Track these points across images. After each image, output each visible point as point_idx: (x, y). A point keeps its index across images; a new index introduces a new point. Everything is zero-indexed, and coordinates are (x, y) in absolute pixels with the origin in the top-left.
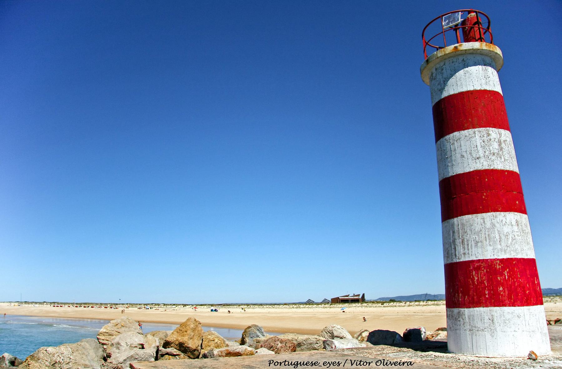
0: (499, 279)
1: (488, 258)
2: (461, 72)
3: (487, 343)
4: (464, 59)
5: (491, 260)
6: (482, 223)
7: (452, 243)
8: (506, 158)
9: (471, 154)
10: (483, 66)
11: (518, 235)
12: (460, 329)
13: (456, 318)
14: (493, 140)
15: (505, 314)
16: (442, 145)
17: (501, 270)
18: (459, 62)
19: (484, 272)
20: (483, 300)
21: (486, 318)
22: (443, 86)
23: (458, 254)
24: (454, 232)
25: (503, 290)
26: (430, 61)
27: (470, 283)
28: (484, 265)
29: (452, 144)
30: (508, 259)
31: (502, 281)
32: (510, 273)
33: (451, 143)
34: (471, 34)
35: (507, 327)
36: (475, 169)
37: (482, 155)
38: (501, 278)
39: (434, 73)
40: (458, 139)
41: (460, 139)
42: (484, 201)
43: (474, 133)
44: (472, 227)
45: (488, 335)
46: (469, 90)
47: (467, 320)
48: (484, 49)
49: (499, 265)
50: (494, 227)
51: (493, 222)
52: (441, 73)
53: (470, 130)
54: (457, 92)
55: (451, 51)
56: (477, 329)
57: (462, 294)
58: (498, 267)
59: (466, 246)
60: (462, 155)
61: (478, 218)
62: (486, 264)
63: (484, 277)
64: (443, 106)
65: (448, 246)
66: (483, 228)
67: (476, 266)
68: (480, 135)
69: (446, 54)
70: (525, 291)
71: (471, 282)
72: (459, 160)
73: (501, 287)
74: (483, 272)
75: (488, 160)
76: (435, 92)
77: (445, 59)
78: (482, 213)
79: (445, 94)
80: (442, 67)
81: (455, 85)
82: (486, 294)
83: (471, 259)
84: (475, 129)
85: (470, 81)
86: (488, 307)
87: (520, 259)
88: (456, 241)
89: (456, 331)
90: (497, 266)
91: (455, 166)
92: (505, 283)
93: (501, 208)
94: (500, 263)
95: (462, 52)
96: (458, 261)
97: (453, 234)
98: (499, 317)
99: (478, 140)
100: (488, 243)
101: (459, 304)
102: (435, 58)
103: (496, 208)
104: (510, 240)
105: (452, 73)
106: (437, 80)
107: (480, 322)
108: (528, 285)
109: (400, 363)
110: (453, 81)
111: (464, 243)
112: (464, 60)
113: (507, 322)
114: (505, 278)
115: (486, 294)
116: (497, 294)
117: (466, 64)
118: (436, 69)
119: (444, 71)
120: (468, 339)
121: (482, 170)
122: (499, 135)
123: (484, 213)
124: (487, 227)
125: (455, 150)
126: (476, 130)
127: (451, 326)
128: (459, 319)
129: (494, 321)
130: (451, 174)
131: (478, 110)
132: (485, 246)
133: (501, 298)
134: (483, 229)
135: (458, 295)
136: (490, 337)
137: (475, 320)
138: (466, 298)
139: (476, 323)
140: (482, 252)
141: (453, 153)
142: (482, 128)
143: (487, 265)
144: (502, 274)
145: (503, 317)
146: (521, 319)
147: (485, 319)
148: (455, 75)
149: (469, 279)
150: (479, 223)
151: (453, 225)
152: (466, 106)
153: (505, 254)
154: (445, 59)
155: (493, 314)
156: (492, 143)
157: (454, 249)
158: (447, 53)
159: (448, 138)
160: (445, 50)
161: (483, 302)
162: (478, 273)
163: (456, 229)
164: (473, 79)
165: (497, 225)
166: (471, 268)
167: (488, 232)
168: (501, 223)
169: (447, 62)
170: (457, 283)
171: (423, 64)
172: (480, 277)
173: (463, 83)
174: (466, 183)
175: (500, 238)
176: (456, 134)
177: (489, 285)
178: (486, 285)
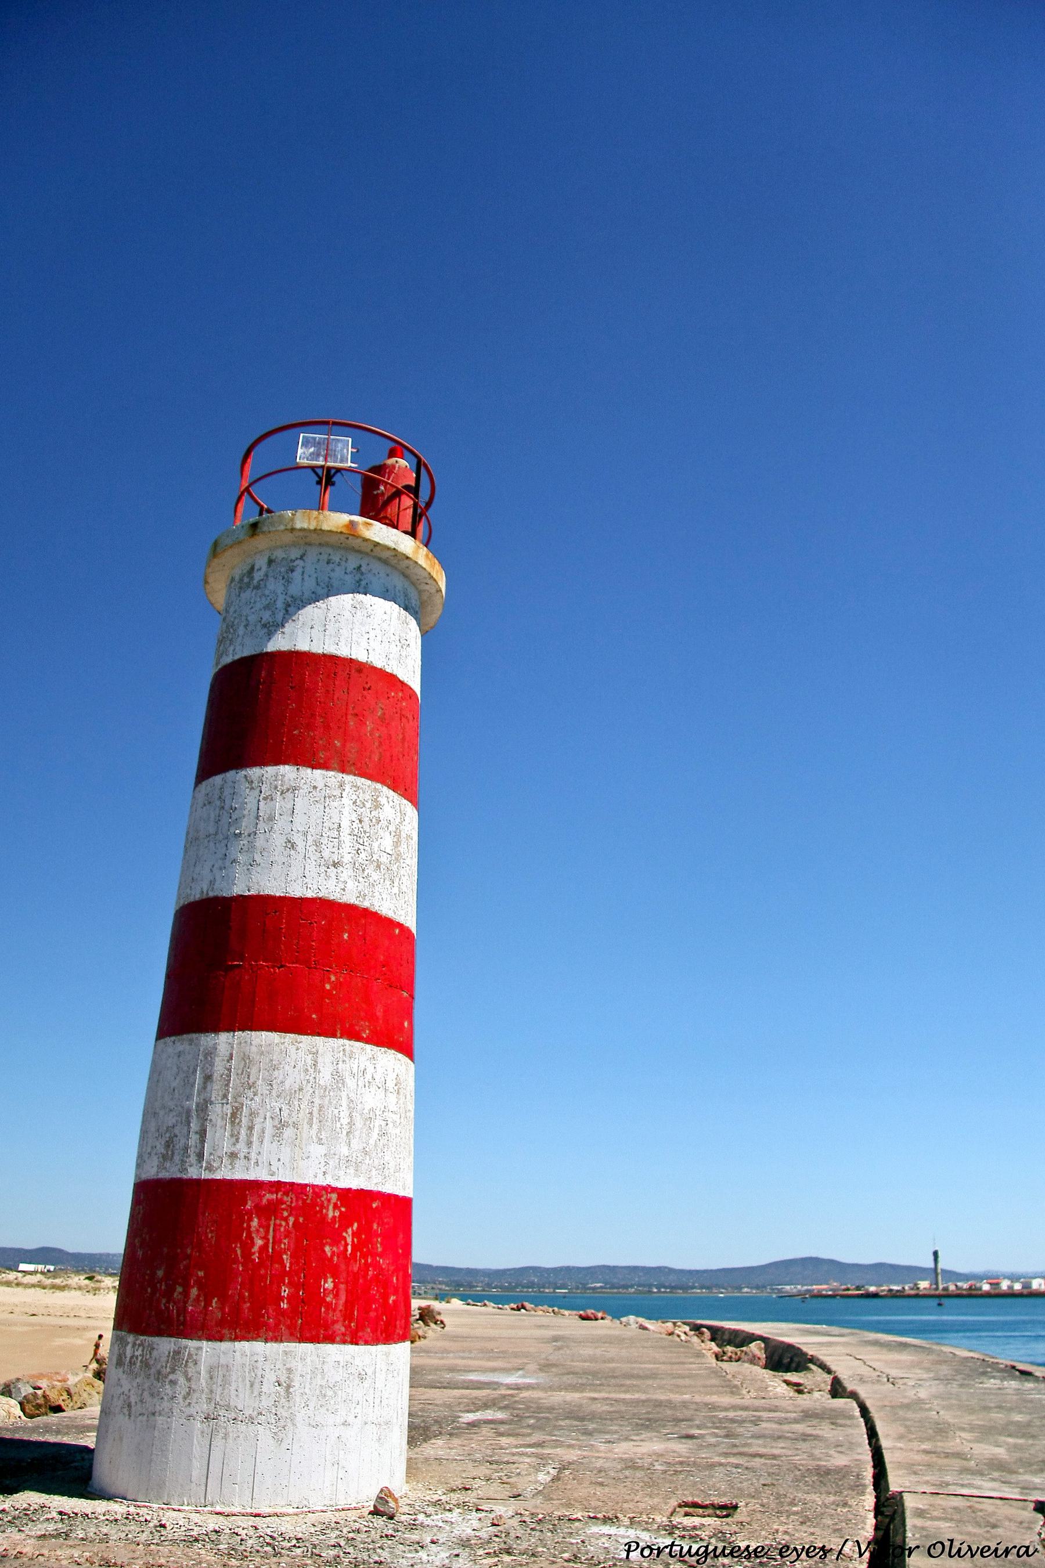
0: (329, 1254)
1: (306, 1182)
2: (346, 600)
3: (258, 1464)
4: (360, 566)
5: (313, 1186)
6: (309, 1068)
7: (194, 1114)
8: (404, 889)
9: (317, 844)
10: (402, 609)
11: (394, 1122)
12: (170, 1414)
13: (159, 1372)
14: (384, 823)
15: (325, 1367)
16: (227, 791)
17: (337, 1226)
18: (346, 569)
19: (288, 1224)
20: (269, 1318)
21: (271, 1377)
22: (279, 616)
23: (211, 1154)
24: (208, 1078)
25: (333, 1290)
26: (265, 529)
27: (236, 1255)
28: (291, 1202)
29: (265, 799)
30: (361, 1192)
31: (335, 1259)
32: (359, 1238)
33: (263, 795)
34: (389, 510)
35: (328, 1410)
36: (320, 895)
37: (347, 859)
38: (335, 1249)
39: (260, 569)
40: (288, 790)
41: (295, 789)
42: (327, 1001)
43: (341, 785)
44: (276, 1073)
45: (264, 1434)
46: (353, 657)
47: (203, 1381)
48: (420, 562)
49: (336, 1207)
50: (340, 1085)
51: (340, 1070)
52: (283, 578)
53: (331, 773)
54: (320, 651)
55: (338, 528)
56: (233, 1415)
57: (199, 1289)
58: (331, 1214)
59: (243, 1132)
60: (290, 842)
61: (298, 1049)
62: (297, 1201)
63: (286, 1241)
64: (263, 674)
65: (174, 1121)
66: (308, 1081)
67: (264, 1201)
68: (354, 797)
69: (321, 530)
70: (385, 1297)
71: (239, 1252)
72: (278, 853)
73: (330, 1280)
74: (284, 1223)
75: (361, 879)
76: (246, 626)
77: (310, 544)
78: (313, 1033)
79: (279, 643)
80: (293, 561)
81: (318, 627)
82: (282, 1298)
83: (251, 1176)
84: (344, 775)
85: (364, 634)
86: (282, 1341)
87: (390, 1195)
88: (210, 1107)
89: (152, 1418)
90: (328, 1209)
91: (259, 869)
92: (343, 1267)
93: (367, 1032)
94: (338, 1200)
95: (365, 544)
96: (205, 1175)
97: (205, 1083)
98: (309, 1377)
99: (346, 811)
100: (314, 1132)
101: (184, 1323)
102: (282, 527)
103: (357, 1028)
104: (375, 1135)
105: (320, 591)
106: (267, 592)
107: (248, 1392)
108: (395, 1279)
109: (996, 1550)
110: (315, 615)
111: (237, 1121)
112: (362, 569)
113: (330, 1393)
114: (346, 1250)
115: (282, 1298)
116: (315, 1298)
117: (363, 583)
118: (270, 562)
119: (297, 575)
120: (197, 1450)
121: (340, 904)
122: (399, 814)
123: (319, 1035)
124: (322, 1083)
125: (271, 818)
126: (349, 778)
127: (133, 1399)
128: (171, 1377)
129: (291, 1390)
130: (239, 889)
131: (366, 724)
132: (304, 1142)
133: (323, 1315)
134: (310, 1085)
135: (186, 1294)
136: (272, 1441)
137: (233, 1384)
138: (214, 1304)
139: (233, 1393)
140: (293, 1159)
141: (262, 826)
142: (363, 779)
143: (300, 1203)
144: (337, 1238)
145: (319, 1376)
146: (366, 1384)
147: (265, 1380)
148: (326, 601)
149: (236, 1243)
150: (300, 1065)
151: (210, 1054)
152: (335, 697)
153: (357, 1176)
154: (310, 544)
155: (293, 1364)
156: (381, 832)
157: (196, 1133)
158: (325, 527)
159: (257, 775)
160: (321, 517)
161: (266, 1324)
162: (269, 1225)
163: (219, 1067)
164: (372, 635)
165: (350, 1083)
166: (248, 1207)
167: (322, 1097)
168: (362, 1078)
169: (312, 554)
170: (189, 1251)
171: (234, 530)
172: (271, 1241)
173: (345, 632)
174: (283, 931)
175: (351, 1124)
176: (287, 771)
177: (294, 1267)
178: (288, 1269)
